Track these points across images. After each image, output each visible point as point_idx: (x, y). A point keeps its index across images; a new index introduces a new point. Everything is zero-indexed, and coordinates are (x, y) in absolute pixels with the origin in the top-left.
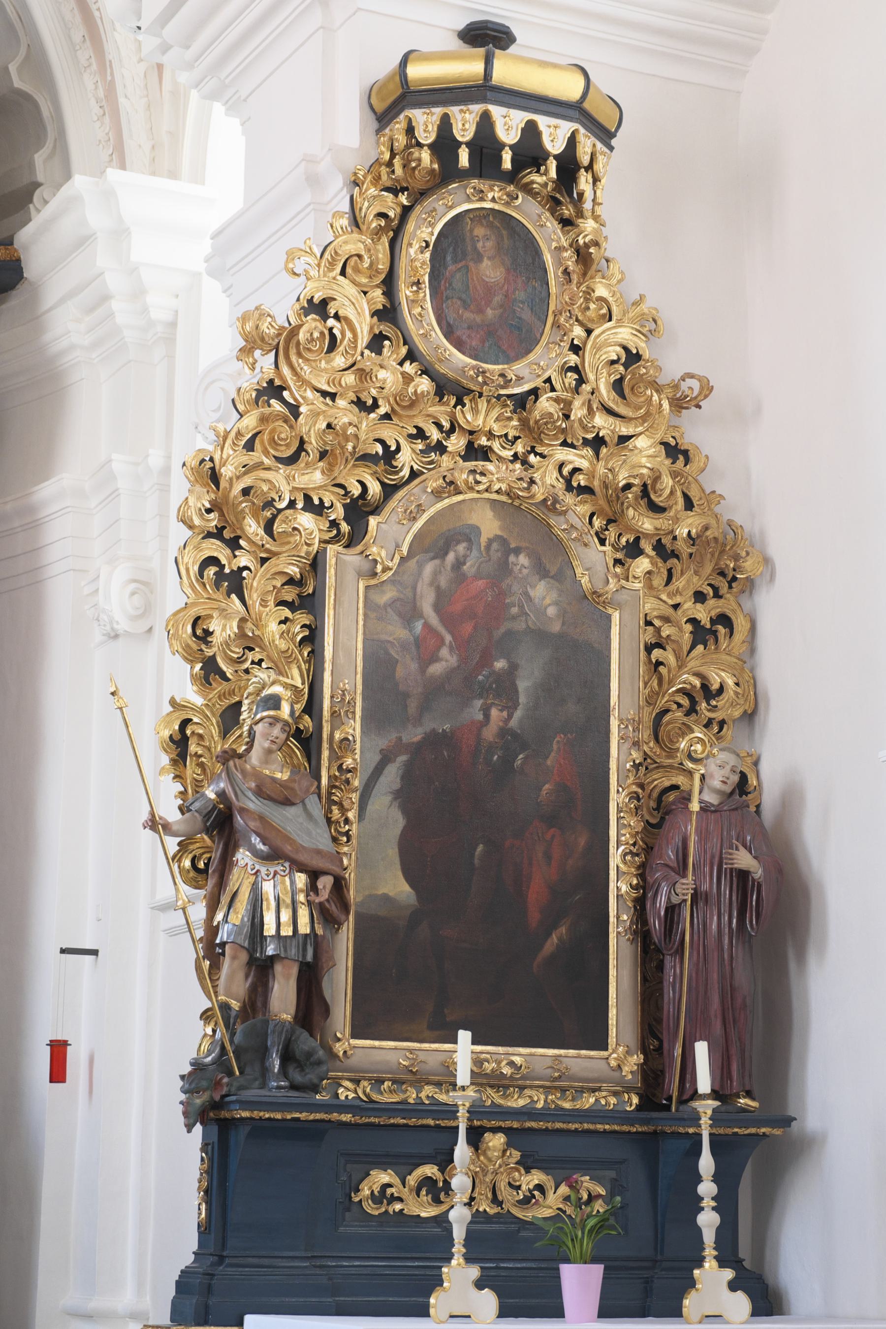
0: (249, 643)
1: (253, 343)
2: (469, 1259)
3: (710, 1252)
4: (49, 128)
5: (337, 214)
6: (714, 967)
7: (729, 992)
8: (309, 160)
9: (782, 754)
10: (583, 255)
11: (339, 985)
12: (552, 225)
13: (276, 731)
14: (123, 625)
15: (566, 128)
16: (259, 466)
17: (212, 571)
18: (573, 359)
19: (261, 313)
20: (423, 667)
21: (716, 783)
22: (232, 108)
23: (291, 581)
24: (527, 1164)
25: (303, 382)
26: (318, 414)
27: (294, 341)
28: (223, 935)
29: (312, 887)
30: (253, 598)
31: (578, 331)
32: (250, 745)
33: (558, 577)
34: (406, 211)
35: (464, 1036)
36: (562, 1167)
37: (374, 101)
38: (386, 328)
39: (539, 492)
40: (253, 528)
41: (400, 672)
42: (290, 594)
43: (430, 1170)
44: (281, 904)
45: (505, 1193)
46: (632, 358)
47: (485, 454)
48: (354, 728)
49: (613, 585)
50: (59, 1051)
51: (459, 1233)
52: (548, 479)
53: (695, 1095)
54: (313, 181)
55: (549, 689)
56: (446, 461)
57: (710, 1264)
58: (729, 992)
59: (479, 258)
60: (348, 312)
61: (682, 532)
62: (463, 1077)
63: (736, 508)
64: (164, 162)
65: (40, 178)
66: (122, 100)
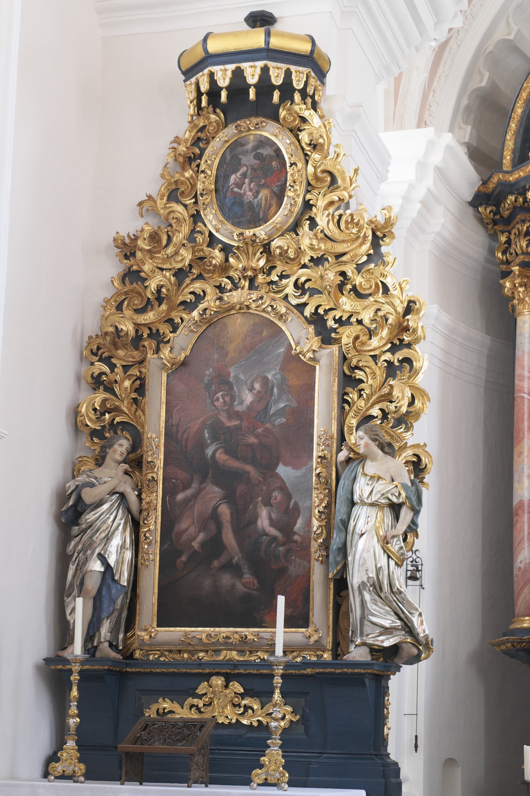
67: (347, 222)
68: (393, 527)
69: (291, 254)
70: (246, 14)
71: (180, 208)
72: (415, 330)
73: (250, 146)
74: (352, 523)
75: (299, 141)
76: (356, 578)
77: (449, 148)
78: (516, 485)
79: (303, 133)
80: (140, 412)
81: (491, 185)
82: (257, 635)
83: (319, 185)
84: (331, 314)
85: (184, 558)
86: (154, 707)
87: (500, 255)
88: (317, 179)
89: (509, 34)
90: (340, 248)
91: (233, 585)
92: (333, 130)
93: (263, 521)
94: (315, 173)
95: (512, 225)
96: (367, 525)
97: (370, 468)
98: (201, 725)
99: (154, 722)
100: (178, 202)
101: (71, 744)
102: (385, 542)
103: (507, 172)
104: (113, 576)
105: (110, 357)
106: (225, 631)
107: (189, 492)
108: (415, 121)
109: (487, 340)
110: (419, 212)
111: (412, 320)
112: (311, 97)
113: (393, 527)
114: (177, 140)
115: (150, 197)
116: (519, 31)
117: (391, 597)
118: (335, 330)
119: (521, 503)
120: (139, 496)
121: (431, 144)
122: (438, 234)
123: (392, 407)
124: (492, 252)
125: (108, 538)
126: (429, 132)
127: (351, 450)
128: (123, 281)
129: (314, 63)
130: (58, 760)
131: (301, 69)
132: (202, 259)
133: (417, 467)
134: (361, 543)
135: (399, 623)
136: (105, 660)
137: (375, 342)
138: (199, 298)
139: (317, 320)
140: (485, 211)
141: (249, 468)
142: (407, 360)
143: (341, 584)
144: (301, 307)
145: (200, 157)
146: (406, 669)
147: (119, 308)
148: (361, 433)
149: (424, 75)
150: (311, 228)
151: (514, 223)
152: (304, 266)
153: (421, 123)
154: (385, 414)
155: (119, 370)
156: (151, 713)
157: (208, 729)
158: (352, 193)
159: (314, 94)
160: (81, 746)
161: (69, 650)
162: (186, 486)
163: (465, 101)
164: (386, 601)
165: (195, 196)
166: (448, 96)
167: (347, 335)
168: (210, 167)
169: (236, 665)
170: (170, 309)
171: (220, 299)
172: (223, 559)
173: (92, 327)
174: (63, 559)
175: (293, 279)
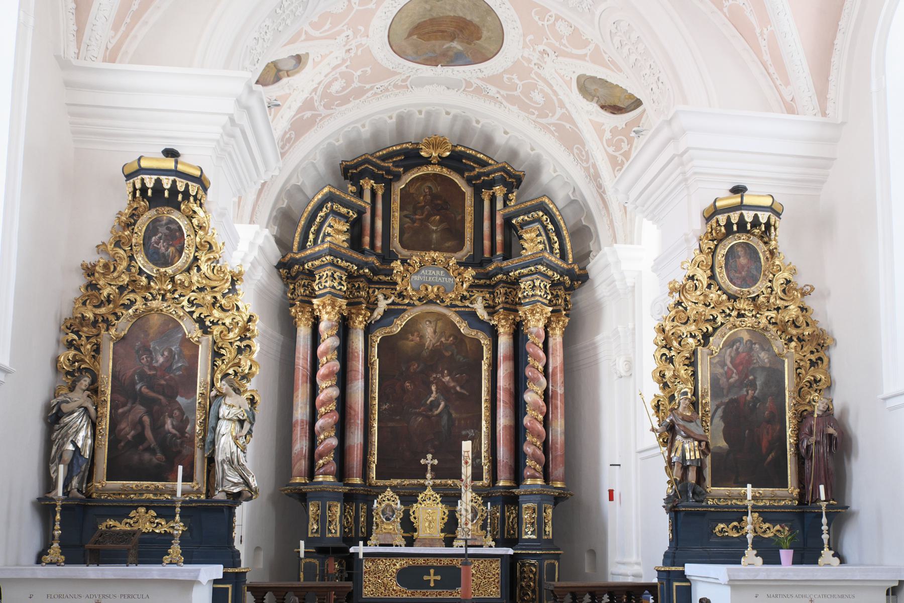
0: (675, 377)
1: (672, 291)
2: (753, 548)
3: (826, 546)
6: (822, 463)
7: (827, 471)
9: (840, 398)
10: (772, 253)
11: (708, 473)
12: (761, 244)
13: (687, 402)
14: (623, 374)
15: (767, 214)
16: (677, 326)
17: (664, 358)
18: (769, 284)
20: (728, 379)
21: (821, 408)
23: (687, 358)
24: (764, 521)
28: (674, 460)
29: (700, 445)
30: (677, 364)
31: (771, 276)
32: (679, 406)
33: (768, 350)
34: (716, 246)
35: (749, 486)
36: (774, 522)
38: (712, 282)
39: (761, 326)
40: (675, 344)
41: (721, 382)
42: (687, 362)
43: (735, 523)
44: (690, 450)
45: (758, 529)
46: (788, 282)
47: (743, 316)
48: (708, 399)
49: (785, 351)
50: (611, 492)
51: (750, 541)
52: (764, 321)
53: (819, 500)
54: (687, 241)
55: (766, 384)
56: (731, 319)
57: (826, 549)
58: (827, 471)
59: (739, 257)
60: (701, 278)
61: (806, 333)
62: (749, 497)
63: (823, 325)
64: (629, 239)
68: (240, 431)
69: (186, 284)
70: (163, 149)
71: (122, 252)
72: (253, 331)
73: (164, 222)
74: (218, 429)
76: (219, 457)
77: (266, 237)
78: (294, 412)
80: (96, 363)
81: (287, 259)
82: (164, 486)
84: (208, 318)
85: (122, 444)
86: (104, 524)
88: (202, 245)
90: (214, 284)
91: (151, 460)
93: (169, 425)
96: (226, 430)
97: (228, 400)
98: (134, 533)
99: (105, 532)
100: (121, 248)
101: (56, 545)
102: (236, 439)
104: (80, 453)
105: (78, 331)
106: (146, 484)
107: (125, 409)
109: (281, 338)
110: (250, 269)
111: (251, 326)
113: (240, 431)
114: (120, 213)
115: (104, 243)
117: (238, 467)
118: (210, 327)
119: (297, 421)
120: (96, 409)
121: (257, 233)
123: (240, 370)
124: (285, 293)
125: (77, 432)
126: (256, 227)
127: (218, 391)
128: (87, 289)
129: (201, 181)
130: (48, 554)
132: (134, 281)
133: (252, 401)
134: (223, 440)
135: (242, 480)
136: (74, 499)
137: (231, 335)
138: (133, 303)
139: (200, 321)
140: (283, 272)
141: (161, 397)
142: (249, 346)
143: (211, 460)
144: (191, 313)
145: (134, 224)
146: (245, 503)
147: (84, 304)
148: (223, 382)
149: (254, 197)
152: (193, 291)
153: (252, 222)
154: (236, 373)
155: (84, 338)
156: (102, 527)
157: (138, 536)
160: (62, 546)
161: (54, 493)
162: (124, 405)
163: (274, 214)
164: (235, 469)
165: (131, 246)
166: (266, 210)
167: (216, 330)
168: (140, 231)
169: (153, 501)
170: (115, 307)
171: (146, 304)
172: (145, 445)
173: (67, 313)
174: (48, 443)
175: (187, 298)
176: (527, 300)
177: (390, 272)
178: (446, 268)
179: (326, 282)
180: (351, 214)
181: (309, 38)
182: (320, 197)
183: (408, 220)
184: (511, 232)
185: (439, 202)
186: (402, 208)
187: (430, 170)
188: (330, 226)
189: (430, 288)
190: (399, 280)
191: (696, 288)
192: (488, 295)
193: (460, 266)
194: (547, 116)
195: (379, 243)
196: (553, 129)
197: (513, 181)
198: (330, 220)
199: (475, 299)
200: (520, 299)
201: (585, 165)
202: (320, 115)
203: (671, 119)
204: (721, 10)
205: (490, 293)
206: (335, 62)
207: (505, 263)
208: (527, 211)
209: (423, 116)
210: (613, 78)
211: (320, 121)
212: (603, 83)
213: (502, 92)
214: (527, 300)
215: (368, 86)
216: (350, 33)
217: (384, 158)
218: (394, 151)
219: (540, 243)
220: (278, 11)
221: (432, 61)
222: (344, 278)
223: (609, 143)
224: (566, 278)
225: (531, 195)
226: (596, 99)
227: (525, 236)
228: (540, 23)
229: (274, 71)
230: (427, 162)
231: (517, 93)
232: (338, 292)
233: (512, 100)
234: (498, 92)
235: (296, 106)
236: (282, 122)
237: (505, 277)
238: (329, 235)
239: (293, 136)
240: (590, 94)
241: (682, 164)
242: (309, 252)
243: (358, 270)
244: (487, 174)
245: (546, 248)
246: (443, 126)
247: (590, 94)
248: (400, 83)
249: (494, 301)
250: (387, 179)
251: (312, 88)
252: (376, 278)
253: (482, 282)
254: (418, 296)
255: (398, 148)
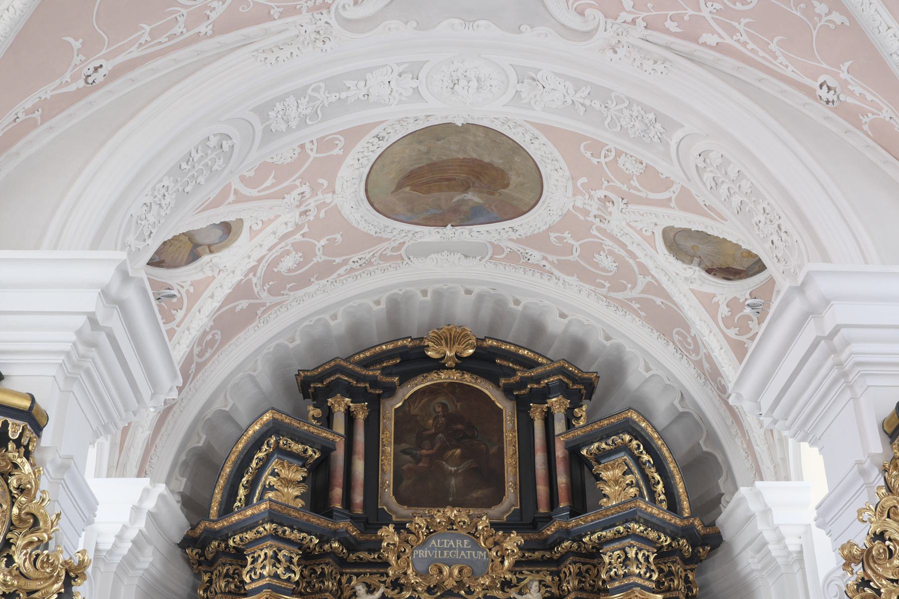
1: (849, 561)
4: (723, 468)
5: (879, 488)
8: (859, 463)
19: (851, 544)
22: (813, 444)
25: (881, 577)
26: (891, 592)
27: (870, 558)
37: (886, 428)
54: (863, 473)
64: (782, 473)
65: (723, 491)
66: (756, 448)
67: (42, 561)
75: (8, 484)
77: (162, 497)
79: (13, 477)
81: (198, 531)
83: (21, 525)
87: (201, 592)
89: (225, 406)
90: (32, 585)
92: (43, 478)
94: (19, 514)
95: (215, 566)
103: (213, 521)
108: (135, 471)
110: (130, 550)
112: (24, 447)
116: (234, 404)
121: (146, 491)
122: (146, 570)
124: (195, 589)
126: (145, 482)
131: (18, 422)
140: (192, 552)
150: (7, 565)
151: (216, 565)
153: (141, 473)
158: (53, 535)
159: (28, 444)
163: (183, 457)
166: (168, 453)
176: (617, 584)
177: (375, 546)
178: (473, 534)
179: (264, 567)
180: (310, 452)
181: (241, 199)
182: (257, 427)
183: (408, 457)
184: (582, 470)
185: (460, 426)
186: (398, 440)
187: (443, 377)
188: (274, 474)
189: (446, 570)
190: (392, 559)
191: (891, 554)
192: (549, 578)
193: (497, 530)
194: (624, 288)
195: (358, 498)
196: (636, 306)
197: (580, 387)
198: (274, 464)
199: (526, 586)
200: (604, 582)
201: (693, 357)
202: (264, 305)
203: (804, 284)
204: (861, 130)
205: (552, 573)
206: (283, 230)
207: (573, 522)
208: (604, 435)
209: (429, 298)
210: (715, 229)
211: (264, 312)
212: (703, 236)
213: (551, 258)
214: (617, 584)
215: (338, 260)
216: (305, 188)
217: (367, 363)
218: (384, 352)
219: (631, 485)
220: (184, 166)
221: (438, 220)
222: (295, 559)
223: (728, 322)
224: (683, 542)
225: (613, 408)
226: (696, 260)
227: (605, 475)
228: (595, 161)
229: (189, 246)
230: (438, 365)
231: (574, 257)
232: (284, 585)
233: (568, 268)
234: (545, 258)
235: (221, 295)
236: (197, 320)
237: (575, 545)
238: (271, 488)
239: (218, 337)
240: (686, 253)
241: (833, 351)
242: (235, 518)
243: (321, 544)
244: (537, 380)
245: (641, 495)
246: (462, 310)
247: (686, 253)
248: (389, 253)
249: (560, 587)
250: (373, 396)
251: (249, 267)
252: (353, 557)
253: (537, 555)
254: (425, 584)
255: (390, 346)
